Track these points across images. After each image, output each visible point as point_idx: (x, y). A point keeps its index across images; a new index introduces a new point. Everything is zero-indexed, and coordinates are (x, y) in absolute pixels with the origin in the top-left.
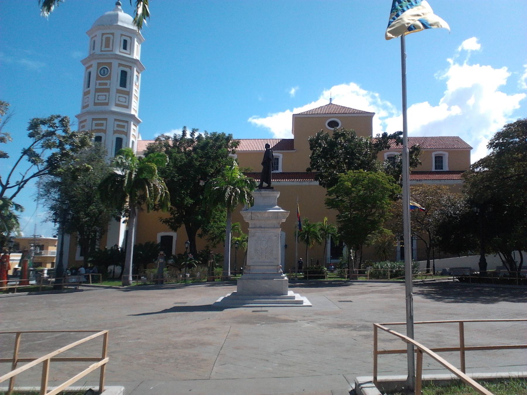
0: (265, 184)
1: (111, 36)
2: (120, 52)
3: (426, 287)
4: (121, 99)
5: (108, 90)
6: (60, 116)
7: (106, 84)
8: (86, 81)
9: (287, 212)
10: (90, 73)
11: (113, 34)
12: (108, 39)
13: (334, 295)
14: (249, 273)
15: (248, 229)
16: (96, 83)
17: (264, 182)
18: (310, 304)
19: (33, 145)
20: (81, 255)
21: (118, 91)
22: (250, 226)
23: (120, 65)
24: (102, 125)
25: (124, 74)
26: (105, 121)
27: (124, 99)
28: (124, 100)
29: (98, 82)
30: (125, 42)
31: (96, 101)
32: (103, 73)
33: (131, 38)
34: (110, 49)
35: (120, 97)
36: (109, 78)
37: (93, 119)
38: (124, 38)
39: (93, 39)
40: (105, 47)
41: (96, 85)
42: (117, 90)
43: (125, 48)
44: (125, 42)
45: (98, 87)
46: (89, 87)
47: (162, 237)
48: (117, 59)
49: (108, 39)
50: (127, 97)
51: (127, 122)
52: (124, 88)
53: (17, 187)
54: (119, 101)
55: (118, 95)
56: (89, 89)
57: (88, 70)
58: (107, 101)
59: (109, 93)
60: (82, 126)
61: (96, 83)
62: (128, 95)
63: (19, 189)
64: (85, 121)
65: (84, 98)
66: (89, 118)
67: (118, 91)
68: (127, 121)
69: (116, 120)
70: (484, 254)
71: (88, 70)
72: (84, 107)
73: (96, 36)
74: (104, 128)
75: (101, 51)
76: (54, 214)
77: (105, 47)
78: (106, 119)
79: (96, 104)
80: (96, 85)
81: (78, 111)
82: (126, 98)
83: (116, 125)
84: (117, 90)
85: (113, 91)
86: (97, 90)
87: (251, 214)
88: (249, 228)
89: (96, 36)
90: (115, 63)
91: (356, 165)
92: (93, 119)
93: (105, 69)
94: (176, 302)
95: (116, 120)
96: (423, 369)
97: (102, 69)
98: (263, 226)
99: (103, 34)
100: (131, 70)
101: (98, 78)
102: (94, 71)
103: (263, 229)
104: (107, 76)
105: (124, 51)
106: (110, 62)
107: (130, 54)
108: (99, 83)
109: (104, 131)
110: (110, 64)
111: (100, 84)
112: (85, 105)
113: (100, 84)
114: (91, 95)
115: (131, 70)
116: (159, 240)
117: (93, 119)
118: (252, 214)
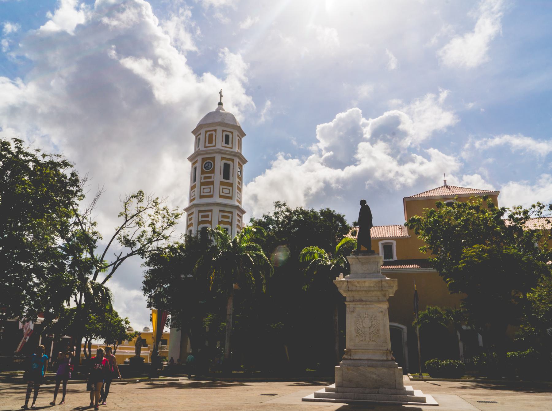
0: (363, 248)
1: (214, 133)
2: (222, 146)
4: (225, 191)
5: (212, 183)
7: (210, 177)
8: (193, 177)
9: (393, 281)
10: (195, 168)
11: (215, 131)
12: (211, 136)
13: (471, 394)
14: (350, 359)
15: (346, 303)
16: (201, 177)
17: (362, 246)
18: (437, 403)
19: (125, 223)
21: (222, 183)
22: (348, 299)
23: (222, 158)
24: (207, 216)
25: (227, 168)
26: (211, 213)
27: (228, 190)
28: (227, 191)
29: (203, 176)
30: (227, 137)
31: (202, 194)
33: (232, 133)
34: (213, 144)
35: (224, 189)
36: (213, 171)
37: (199, 211)
39: (198, 137)
40: (209, 143)
41: (201, 179)
42: (221, 182)
44: (227, 137)
45: (203, 180)
46: (195, 182)
47: (167, 340)
49: (211, 136)
50: (231, 188)
51: (231, 213)
52: (228, 180)
53: (113, 266)
54: (223, 192)
55: (222, 187)
56: (195, 183)
58: (211, 193)
60: (190, 219)
61: (201, 177)
62: (231, 187)
63: (114, 269)
64: (192, 213)
65: (191, 192)
66: (195, 210)
67: (222, 183)
68: (411, 380)
69: (220, 211)
72: (191, 201)
73: (200, 134)
74: (209, 219)
75: (205, 147)
76: (149, 297)
77: (209, 143)
78: (211, 211)
79: (201, 197)
80: (201, 179)
81: (187, 204)
82: (229, 189)
83: (220, 216)
84: (221, 182)
86: (202, 184)
87: (347, 284)
88: (346, 301)
90: (218, 157)
91: (477, 201)
92: (200, 211)
93: (210, 164)
94: (270, 394)
95: (220, 211)
97: (207, 162)
98: (364, 299)
99: (206, 132)
100: (233, 163)
101: (203, 172)
102: (199, 165)
103: (364, 303)
104: (210, 170)
105: (227, 145)
106: (214, 156)
107: (232, 148)
108: (204, 177)
109: (231, 224)
110: (213, 159)
111: (205, 178)
112: (192, 198)
113: (205, 178)
114: (197, 189)
115: (233, 163)
117: (200, 211)
118: (349, 283)
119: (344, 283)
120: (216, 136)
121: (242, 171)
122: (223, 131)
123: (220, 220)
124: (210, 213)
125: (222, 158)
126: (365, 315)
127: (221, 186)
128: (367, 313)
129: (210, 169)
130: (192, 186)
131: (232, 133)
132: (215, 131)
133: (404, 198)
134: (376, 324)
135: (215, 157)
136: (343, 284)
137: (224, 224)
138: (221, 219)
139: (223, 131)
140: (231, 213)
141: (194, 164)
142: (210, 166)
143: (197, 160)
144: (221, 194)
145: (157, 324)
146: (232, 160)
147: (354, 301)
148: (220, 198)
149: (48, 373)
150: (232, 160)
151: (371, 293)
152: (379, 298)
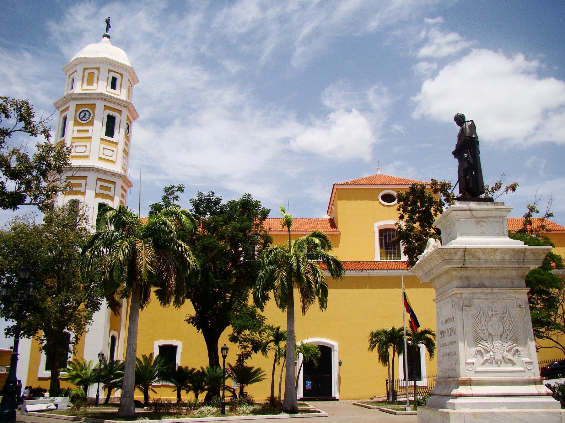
3: (292, 370)
4: (106, 152)
6: (553, 214)
20: (47, 369)
23: (106, 107)
28: (110, 153)
30: (114, 80)
32: (82, 116)
38: (112, 74)
39: (72, 76)
43: (113, 87)
44: (114, 80)
47: (162, 348)
48: (74, 99)
57: (64, 115)
59: (91, 143)
69: (98, 179)
70: (150, 287)
71: (64, 115)
73: (76, 71)
82: (113, 151)
83: (98, 187)
84: (102, 139)
85: (96, 140)
89: (76, 71)
93: (87, 113)
95: (98, 179)
96: (49, 381)
99: (85, 69)
105: (112, 91)
107: (119, 95)
116: (156, 352)
118: (466, 253)
119: (458, 252)
120: (98, 76)
121: (131, 129)
122: (110, 71)
123: (98, 192)
124: (83, 181)
125: (106, 107)
126: (490, 313)
127: (101, 145)
128: (493, 309)
129: (87, 120)
130: (58, 142)
131: (122, 75)
132: (98, 69)
133: (334, 185)
134: (510, 328)
135: (95, 104)
136: (456, 253)
137: (102, 197)
138: (99, 191)
139: (110, 71)
140: (114, 183)
141: (64, 113)
142: (87, 116)
143: (68, 107)
144: (116, 149)
145: (476, 236)
146: (120, 112)
147: (469, 286)
148: (99, 161)
149: (55, 416)
150: (120, 112)
151: (501, 271)
152: (513, 282)
